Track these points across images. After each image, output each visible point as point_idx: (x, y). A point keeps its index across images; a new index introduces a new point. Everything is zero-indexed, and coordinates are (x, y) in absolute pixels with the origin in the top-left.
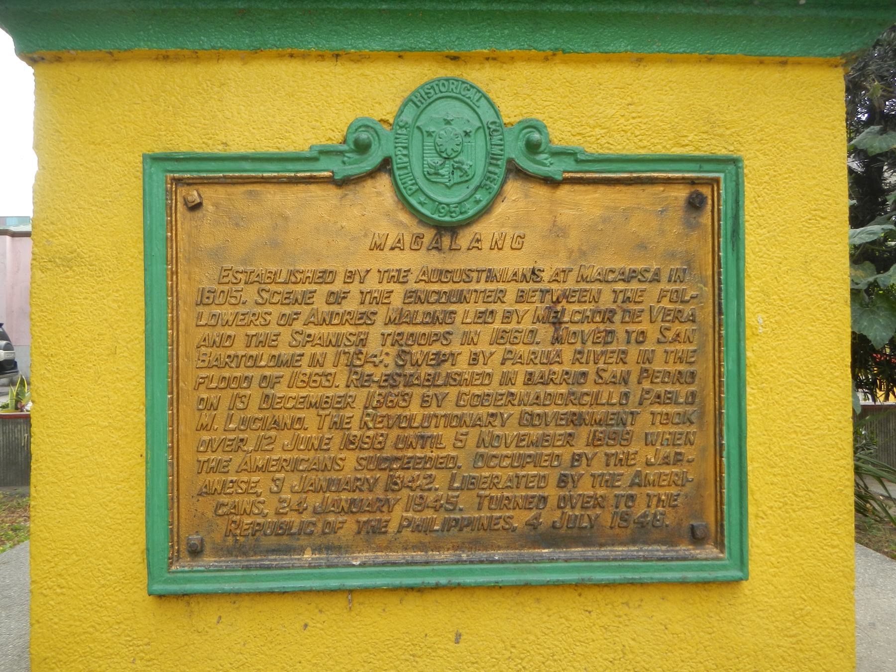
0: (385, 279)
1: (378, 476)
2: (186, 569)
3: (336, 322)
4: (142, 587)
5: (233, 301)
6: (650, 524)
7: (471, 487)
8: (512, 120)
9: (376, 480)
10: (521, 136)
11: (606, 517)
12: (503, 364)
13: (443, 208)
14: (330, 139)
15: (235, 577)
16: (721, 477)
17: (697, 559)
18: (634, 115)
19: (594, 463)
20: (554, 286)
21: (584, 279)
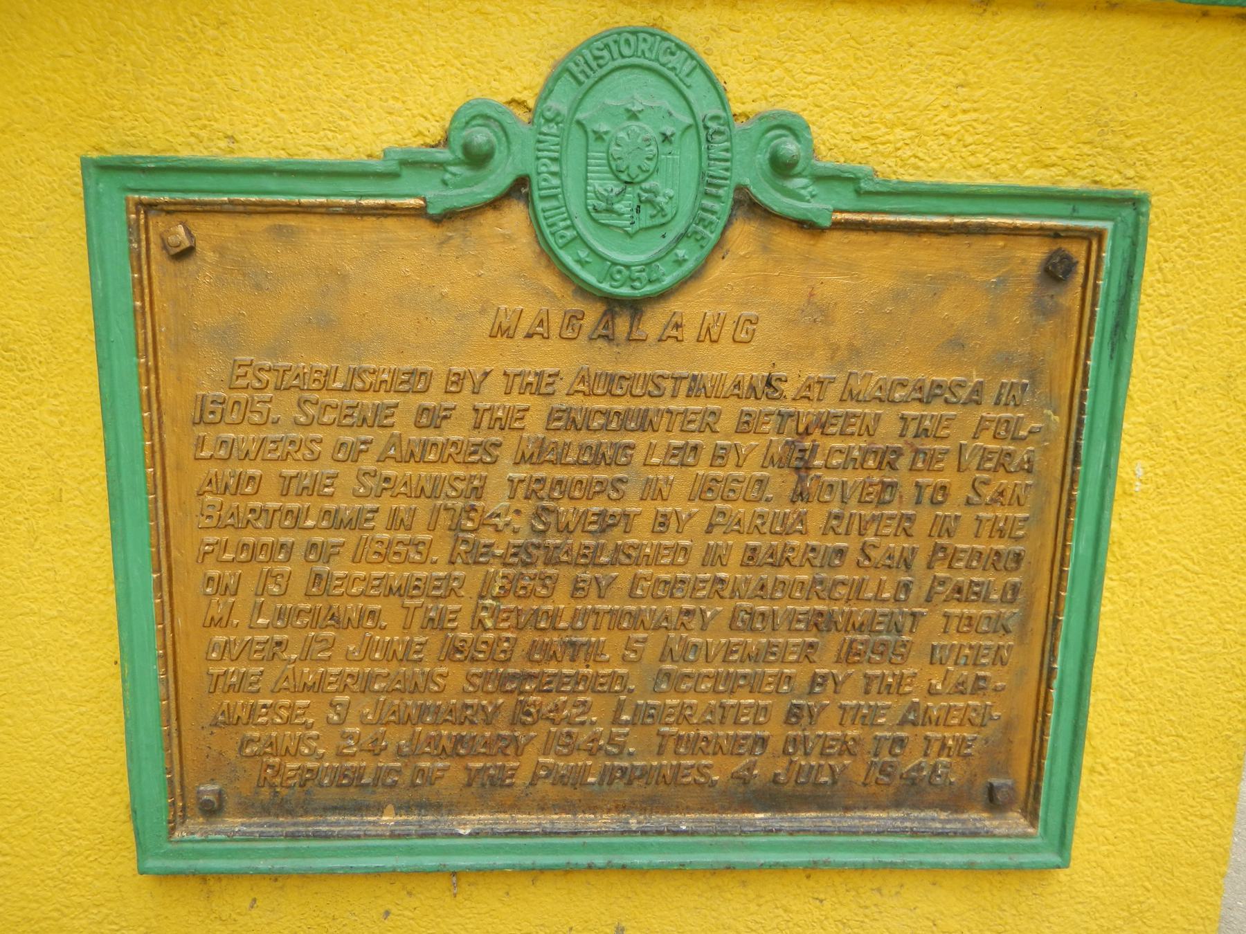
8: (748, 108)
10: (763, 143)
13: (619, 272)
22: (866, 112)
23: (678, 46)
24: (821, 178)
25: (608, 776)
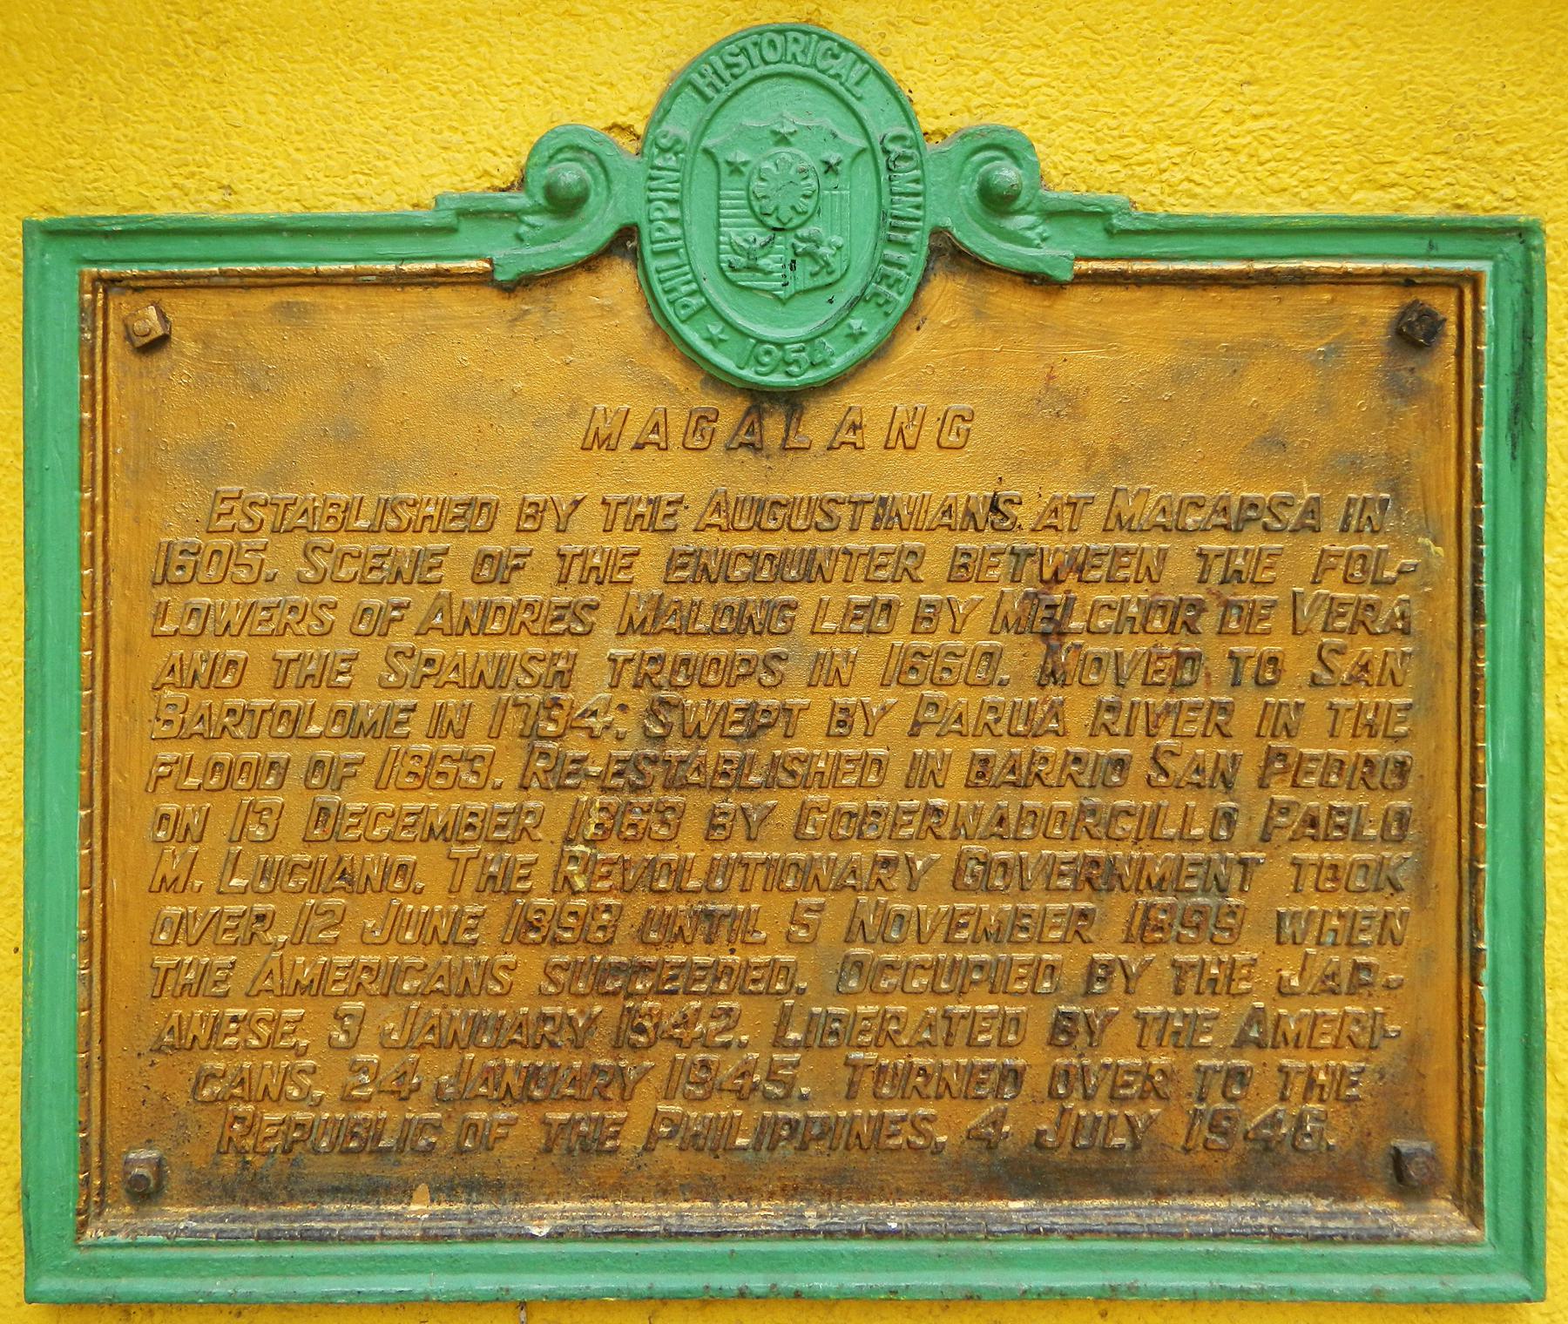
0: (620, 523)
1: (597, 1009)
2: (120, 1238)
3: (496, 627)
4: (16, 1271)
5: (243, 574)
6: (1288, 1141)
7: (832, 1041)
8: (944, 123)
9: (592, 1020)
10: (968, 169)
11: (1174, 1128)
12: (913, 735)
13: (768, 353)
14: (486, 173)
15: (240, 1261)
16: (1474, 1032)
17: (1411, 1242)
18: (1256, 109)
19: (1145, 985)
20: (1047, 541)
21: (1119, 522)
22: (1113, 123)
23: (841, 45)
24: (1055, 214)
25: (768, 1134)
